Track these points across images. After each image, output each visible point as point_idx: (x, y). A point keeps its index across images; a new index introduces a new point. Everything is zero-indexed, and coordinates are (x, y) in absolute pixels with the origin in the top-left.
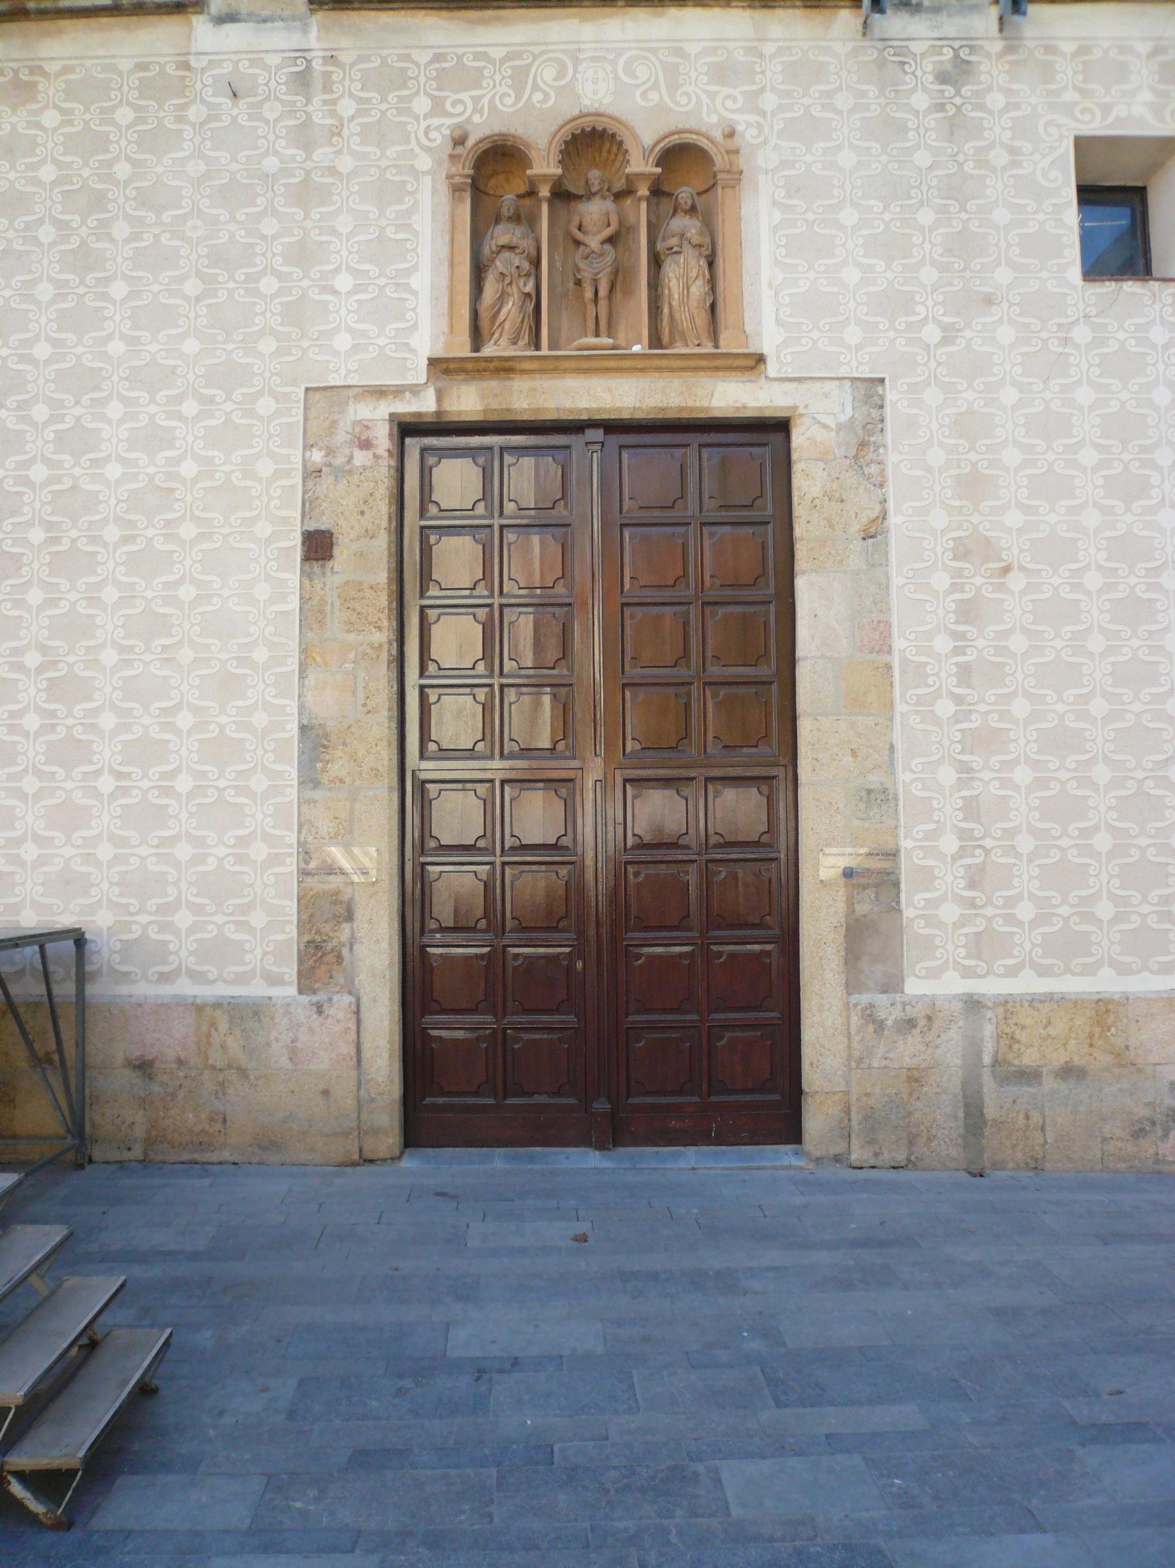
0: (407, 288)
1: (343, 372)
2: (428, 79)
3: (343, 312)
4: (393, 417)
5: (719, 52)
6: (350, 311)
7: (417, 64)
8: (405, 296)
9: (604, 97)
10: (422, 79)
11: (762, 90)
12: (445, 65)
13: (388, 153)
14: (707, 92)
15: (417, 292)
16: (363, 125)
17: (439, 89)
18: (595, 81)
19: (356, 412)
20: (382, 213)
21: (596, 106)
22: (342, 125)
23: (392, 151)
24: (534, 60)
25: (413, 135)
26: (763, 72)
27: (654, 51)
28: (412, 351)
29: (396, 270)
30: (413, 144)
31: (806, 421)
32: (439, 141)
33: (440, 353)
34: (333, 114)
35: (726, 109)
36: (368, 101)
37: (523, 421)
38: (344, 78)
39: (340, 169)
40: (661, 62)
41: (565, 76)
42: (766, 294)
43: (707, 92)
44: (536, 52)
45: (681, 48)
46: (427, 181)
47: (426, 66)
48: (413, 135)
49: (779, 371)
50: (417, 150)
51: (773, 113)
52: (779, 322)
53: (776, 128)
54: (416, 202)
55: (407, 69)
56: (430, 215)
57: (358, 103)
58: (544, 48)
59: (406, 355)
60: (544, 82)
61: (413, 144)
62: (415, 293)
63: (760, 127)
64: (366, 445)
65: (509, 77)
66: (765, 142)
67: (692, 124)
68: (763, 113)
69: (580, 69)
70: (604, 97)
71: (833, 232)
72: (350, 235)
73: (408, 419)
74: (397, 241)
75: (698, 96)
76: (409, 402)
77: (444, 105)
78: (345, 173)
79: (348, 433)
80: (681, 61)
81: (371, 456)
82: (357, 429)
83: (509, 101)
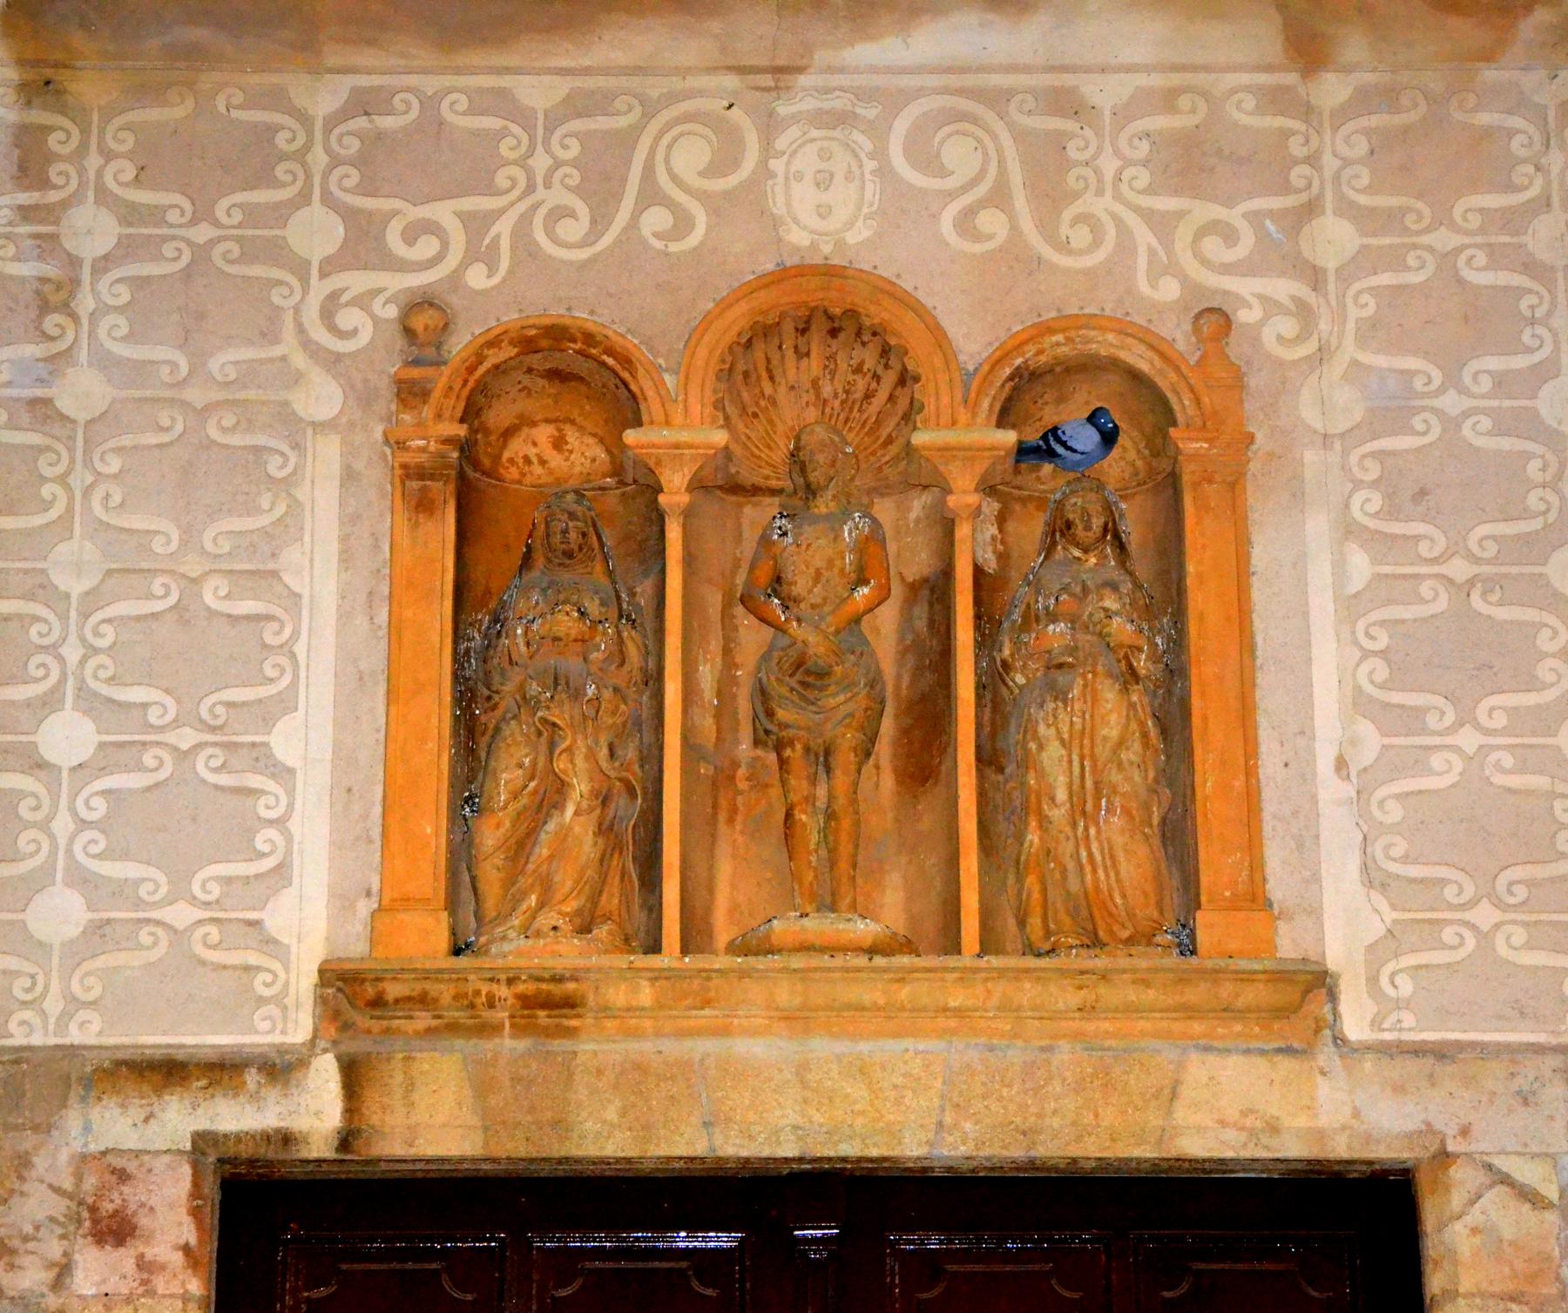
0: (262, 759)
1: (53, 1005)
2: (336, 161)
3: (63, 824)
4: (203, 1141)
5: (1184, 102)
6: (83, 824)
7: (305, 120)
8: (255, 781)
9: (850, 225)
10: (318, 158)
11: (1311, 209)
12: (387, 122)
13: (214, 365)
14: (1148, 215)
15: (291, 771)
16: (139, 283)
17: (368, 188)
18: (824, 181)
19: (87, 1128)
20: (189, 536)
21: (827, 249)
22: (75, 282)
23: (223, 362)
24: (648, 115)
25: (288, 318)
26: (1313, 160)
27: (998, 99)
28: (269, 944)
29: (230, 705)
30: (288, 345)
31: (1463, 1177)
32: (365, 337)
33: (355, 947)
34: (48, 244)
35: (1205, 262)
36: (156, 215)
37: (603, 1161)
38: (83, 147)
39: (64, 404)
40: (1020, 136)
41: (736, 164)
42: (1331, 790)
43: (1148, 215)
44: (654, 94)
45: (1072, 91)
46: (328, 454)
47: (331, 123)
48: (288, 318)
49: (1376, 1023)
50: (299, 360)
51: (1346, 274)
52: (1373, 878)
53: (1353, 313)
54: (295, 506)
55: (274, 129)
56: (334, 546)
57: (124, 221)
58: (677, 83)
59: (253, 959)
60: (674, 178)
61: (288, 345)
62: (284, 774)
63: (1304, 312)
64: (115, 1230)
65: (574, 163)
66: (1322, 355)
67: (1105, 302)
68: (1315, 277)
69: (781, 143)
70: (850, 225)
71: (1530, 614)
72: (92, 600)
73: (245, 1151)
74: (233, 619)
75: (1119, 222)
76: (255, 1098)
77: (380, 238)
78: (82, 417)
79: (57, 1190)
80: (1070, 125)
81: (129, 1265)
82: (90, 1182)
83: (572, 230)
